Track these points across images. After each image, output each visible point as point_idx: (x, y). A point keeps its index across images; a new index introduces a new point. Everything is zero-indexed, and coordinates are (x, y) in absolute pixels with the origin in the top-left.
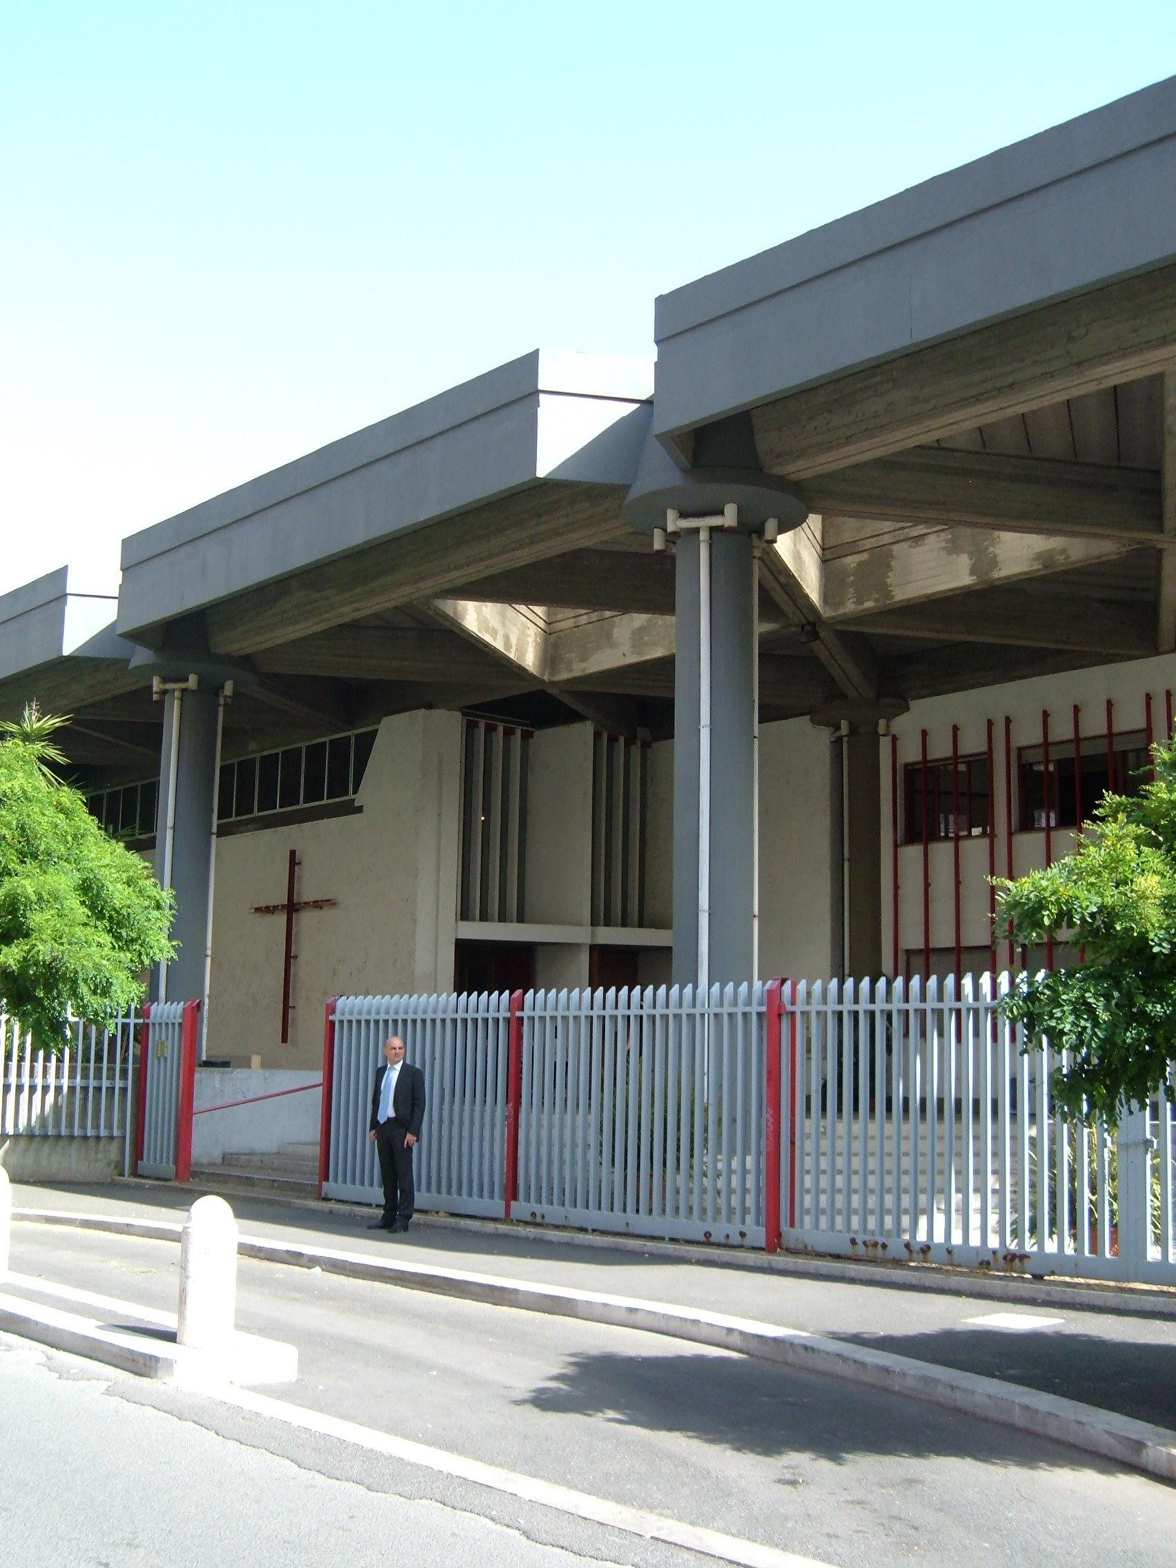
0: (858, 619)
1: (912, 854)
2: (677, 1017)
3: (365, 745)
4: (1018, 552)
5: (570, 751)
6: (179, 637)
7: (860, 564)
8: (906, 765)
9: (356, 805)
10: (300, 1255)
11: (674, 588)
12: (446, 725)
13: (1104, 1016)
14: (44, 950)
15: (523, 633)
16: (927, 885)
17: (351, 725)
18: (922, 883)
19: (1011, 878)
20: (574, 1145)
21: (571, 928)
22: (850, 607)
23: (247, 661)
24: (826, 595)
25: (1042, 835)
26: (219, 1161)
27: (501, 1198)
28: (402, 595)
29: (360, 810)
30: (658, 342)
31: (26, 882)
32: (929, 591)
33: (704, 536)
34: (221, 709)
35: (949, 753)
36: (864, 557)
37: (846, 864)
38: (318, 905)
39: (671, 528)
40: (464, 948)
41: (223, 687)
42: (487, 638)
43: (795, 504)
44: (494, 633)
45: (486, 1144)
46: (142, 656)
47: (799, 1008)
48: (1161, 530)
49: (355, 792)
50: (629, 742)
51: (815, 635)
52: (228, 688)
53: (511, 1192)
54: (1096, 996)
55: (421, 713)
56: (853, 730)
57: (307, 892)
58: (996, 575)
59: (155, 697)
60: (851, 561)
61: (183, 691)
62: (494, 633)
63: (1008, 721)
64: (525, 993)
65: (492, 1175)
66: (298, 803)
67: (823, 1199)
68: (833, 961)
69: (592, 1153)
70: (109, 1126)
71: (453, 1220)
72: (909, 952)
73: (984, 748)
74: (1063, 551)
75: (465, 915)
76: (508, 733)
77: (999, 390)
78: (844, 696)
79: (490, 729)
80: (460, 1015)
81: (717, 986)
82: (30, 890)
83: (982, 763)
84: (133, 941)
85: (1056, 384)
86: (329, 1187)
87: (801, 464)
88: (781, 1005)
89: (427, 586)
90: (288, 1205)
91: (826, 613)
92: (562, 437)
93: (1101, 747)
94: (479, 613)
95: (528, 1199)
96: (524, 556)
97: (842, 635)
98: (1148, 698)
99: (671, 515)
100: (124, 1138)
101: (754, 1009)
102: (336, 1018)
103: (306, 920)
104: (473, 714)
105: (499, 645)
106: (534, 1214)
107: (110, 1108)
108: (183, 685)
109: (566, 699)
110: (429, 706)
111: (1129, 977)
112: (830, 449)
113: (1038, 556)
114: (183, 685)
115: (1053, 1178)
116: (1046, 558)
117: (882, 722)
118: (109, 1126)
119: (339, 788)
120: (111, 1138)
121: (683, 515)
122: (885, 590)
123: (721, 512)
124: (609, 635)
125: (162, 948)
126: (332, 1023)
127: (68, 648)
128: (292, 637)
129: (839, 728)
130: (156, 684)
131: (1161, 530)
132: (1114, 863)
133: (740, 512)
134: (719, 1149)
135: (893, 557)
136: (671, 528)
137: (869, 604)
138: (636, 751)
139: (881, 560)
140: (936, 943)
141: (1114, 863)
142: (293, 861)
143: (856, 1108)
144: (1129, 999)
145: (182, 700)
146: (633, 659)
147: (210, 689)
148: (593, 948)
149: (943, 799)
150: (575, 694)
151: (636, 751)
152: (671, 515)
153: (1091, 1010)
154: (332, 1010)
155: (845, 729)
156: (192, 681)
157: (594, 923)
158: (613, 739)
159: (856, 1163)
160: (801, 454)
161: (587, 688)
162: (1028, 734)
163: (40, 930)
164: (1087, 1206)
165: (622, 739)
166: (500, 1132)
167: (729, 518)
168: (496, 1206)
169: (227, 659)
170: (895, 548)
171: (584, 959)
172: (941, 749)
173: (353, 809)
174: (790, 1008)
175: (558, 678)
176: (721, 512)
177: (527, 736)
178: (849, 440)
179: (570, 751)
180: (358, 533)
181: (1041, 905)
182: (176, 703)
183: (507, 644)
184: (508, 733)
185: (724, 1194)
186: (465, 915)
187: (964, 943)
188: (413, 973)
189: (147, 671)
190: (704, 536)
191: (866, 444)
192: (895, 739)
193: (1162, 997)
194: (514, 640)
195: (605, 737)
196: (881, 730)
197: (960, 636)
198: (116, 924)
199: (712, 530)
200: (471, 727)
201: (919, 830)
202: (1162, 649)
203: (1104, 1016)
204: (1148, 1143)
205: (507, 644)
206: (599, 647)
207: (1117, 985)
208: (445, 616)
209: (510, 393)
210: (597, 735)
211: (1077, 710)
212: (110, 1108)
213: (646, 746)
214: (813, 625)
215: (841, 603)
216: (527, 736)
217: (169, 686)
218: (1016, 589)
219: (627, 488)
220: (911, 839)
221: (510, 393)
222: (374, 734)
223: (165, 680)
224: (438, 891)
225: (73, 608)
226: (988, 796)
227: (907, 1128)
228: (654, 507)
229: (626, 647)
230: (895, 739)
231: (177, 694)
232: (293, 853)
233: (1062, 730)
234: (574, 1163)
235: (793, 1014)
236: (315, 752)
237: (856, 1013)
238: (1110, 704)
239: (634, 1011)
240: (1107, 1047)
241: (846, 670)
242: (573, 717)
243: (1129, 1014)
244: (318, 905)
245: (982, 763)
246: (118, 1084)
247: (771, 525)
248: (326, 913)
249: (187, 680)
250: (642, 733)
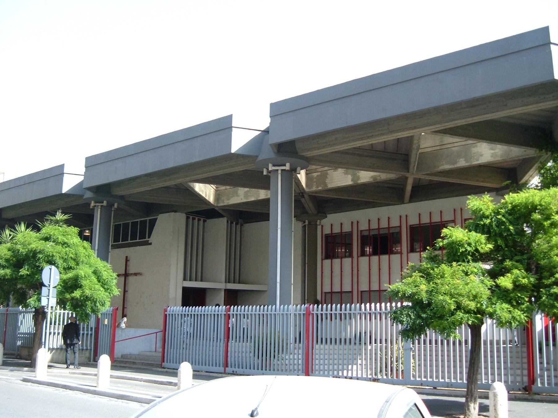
0: (316, 192)
1: (327, 262)
2: (267, 315)
3: (153, 223)
4: (366, 176)
5: (219, 228)
6: (102, 191)
7: (317, 176)
8: (326, 234)
9: (150, 242)
10: (172, 383)
11: (269, 184)
12: (181, 217)
13: (413, 317)
14: (88, 292)
15: (210, 191)
16: (332, 272)
17: (148, 217)
18: (334, 273)
19: (390, 284)
20: (235, 352)
21: (218, 283)
22: (314, 189)
23: (122, 197)
24: (307, 185)
25: (368, 258)
26: (120, 357)
27: (223, 367)
28: (180, 181)
29: (151, 244)
30: (270, 117)
31: (80, 271)
32: (339, 185)
33: (280, 172)
34: (113, 212)
35: (340, 231)
36: (319, 173)
37: (306, 265)
38: (136, 274)
39: (270, 169)
40: (185, 290)
41: (114, 205)
42: (201, 193)
43: (306, 162)
44: (202, 191)
45: (204, 351)
46: (88, 195)
47: (315, 312)
48: (408, 172)
49: (149, 238)
50: (237, 224)
51: (303, 197)
52: (116, 205)
53: (226, 365)
54: (411, 313)
55: (173, 213)
56: (309, 223)
57: (131, 270)
58: (359, 182)
59: (91, 207)
60: (315, 175)
61: (102, 206)
62: (202, 191)
63: (358, 222)
64: (230, 307)
65: (219, 361)
66: (128, 240)
67: (322, 366)
68: (302, 296)
69: (252, 355)
70: (86, 346)
71: (208, 374)
72: (325, 293)
73: (350, 230)
74: (379, 176)
75: (185, 279)
76: (199, 220)
77: (368, 137)
78: (307, 213)
79: (194, 219)
80: (184, 313)
81: (282, 306)
82: (83, 274)
83: (350, 234)
84: (108, 289)
85: (385, 137)
86: (164, 364)
87: (309, 153)
88: (310, 312)
89: (188, 179)
90: (151, 370)
91: (307, 190)
92: (239, 141)
93: (386, 231)
94: (199, 186)
95: (231, 367)
96: (221, 172)
97: (310, 196)
98: (400, 217)
99: (270, 165)
100: (91, 349)
101: (302, 312)
102: (167, 313)
103: (131, 279)
104: (189, 215)
105: (204, 195)
106: (233, 371)
107: (87, 340)
108: (102, 204)
109: (220, 212)
110: (175, 212)
111: (418, 308)
112: (318, 149)
113: (372, 177)
114: (102, 204)
115: (386, 359)
116: (374, 178)
117: (318, 221)
118: (86, 346)
119: (143, 236)
120: (87, 349)
121: (274, 166)
122: (325, 184)
123: (285, 165)
124: (237, 192)
125: (117, 292)
126: (166, 315)
127: (64, 191)
128: (139, 191)
129: (304, 222)
130: (93, 204)
131: (408, 172)
132: (415, 281)
133: (291, 165)
134: (287, 353)
135: (328, 174)
136: (270, 169)
137: (320, 188)
138: (238, 226)
139: (325, 175)
140: (334, 290)
141: (415, 281)
142: (127, 260)
143: (317, 342)
144: (418, 312)
145: (101, 209)
146: (244, 200)
147: (110, 205)
148: (225, 290)
149: (337, 245)
150: (223, 210)
151: (238, 226)
152: (270, 165)
153: (410, 316)
154: (166, 310)
155: (307, 223)
156: (105, 203)
157: (226, 282)
158: (232, 223)
159: (322, 357)
160: (309, 150)
161: (227, 208)
162: (364, 226)
163: (86, 286)
164: (395, 366)
165: (234, 223)
166: (222, 348)
167: (287, 167)
168: (221, 369)
169: (116, 196)
170: (329, 171)
171: (223, 293)
172: (337, 230)
173: (148, 243)
174: (312, 312)
175: (219, 205)
176: (285, 165)
177: (204, 221)
178: (324, 147)
179: (219, 228)
180: (171, 163)
181: (398, 292)
182: (99, 210)
183: (206, 195)
184: (199, 220)
185: (288, 366)
186: (185, 279)
187: (343, 291)
188: (168, 297)
189: (90, 199)
190: (280, 172)
191: (329, 149)
192: (322, 226)
193: (425, 313)
194: (208, 194)
195: (229, 222)
196: (318, 223)
197: (345, 197)
198: (104, 284)
199: (282, 170)
200: (188, 218)
201: (330, 255)
202: (405, 202)
203: (413, 317)
204: (411, 349)
205: (206, 195)
206: (233, 196)
207: (415, 310)
208: (191, 187)
209: (223, 126)
210: (227, 222)
211: (379, 219)
212: (87, 340)
213: (242, 225)
214: (302, 193)
215: (312, 187)
216: (204, 221)
217: (97, 204)
218: (364, 185)
219: (257, 157)
220: (327, 258)
221: (223, 126)
222: (156, 219)
223: (96, 202)
224: (177, 271)
225: (66, 178)
226: (351, 244)
227: (331, 347)
228: (265, 163)
229: (242, 197)
230: (322, 226)
231: (99, 207)
232: (127, 257)
233: (374, 226)
234: (235, 357)
235: (313, 314)
236: (135, 224)
237: (331, 314)
238: (389, 218)
239: (239, 313)
240: (414, 323)
241: (310, 206)
242: (222, 216)
243: (419, 316)
244: (136, 274)
245: (350, 234)
246: (90, 333)
247: (299, 169)
248: (138, 277)
249: (103, 203)
250: (241, 221)
